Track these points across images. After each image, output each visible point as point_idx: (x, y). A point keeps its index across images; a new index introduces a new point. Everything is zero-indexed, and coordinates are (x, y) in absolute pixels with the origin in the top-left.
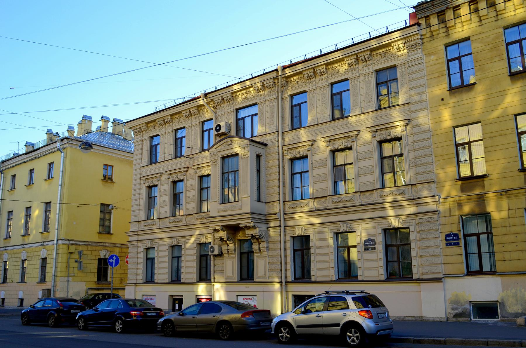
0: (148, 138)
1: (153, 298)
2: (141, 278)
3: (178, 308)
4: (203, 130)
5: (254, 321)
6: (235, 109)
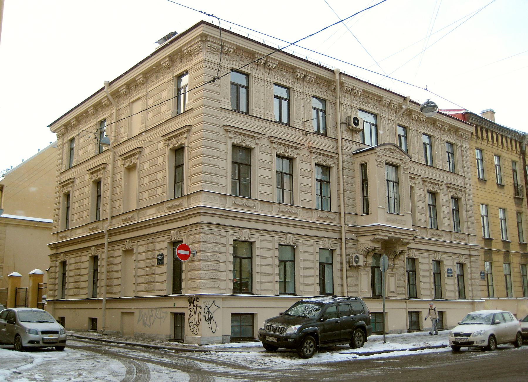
6: (175, 76)
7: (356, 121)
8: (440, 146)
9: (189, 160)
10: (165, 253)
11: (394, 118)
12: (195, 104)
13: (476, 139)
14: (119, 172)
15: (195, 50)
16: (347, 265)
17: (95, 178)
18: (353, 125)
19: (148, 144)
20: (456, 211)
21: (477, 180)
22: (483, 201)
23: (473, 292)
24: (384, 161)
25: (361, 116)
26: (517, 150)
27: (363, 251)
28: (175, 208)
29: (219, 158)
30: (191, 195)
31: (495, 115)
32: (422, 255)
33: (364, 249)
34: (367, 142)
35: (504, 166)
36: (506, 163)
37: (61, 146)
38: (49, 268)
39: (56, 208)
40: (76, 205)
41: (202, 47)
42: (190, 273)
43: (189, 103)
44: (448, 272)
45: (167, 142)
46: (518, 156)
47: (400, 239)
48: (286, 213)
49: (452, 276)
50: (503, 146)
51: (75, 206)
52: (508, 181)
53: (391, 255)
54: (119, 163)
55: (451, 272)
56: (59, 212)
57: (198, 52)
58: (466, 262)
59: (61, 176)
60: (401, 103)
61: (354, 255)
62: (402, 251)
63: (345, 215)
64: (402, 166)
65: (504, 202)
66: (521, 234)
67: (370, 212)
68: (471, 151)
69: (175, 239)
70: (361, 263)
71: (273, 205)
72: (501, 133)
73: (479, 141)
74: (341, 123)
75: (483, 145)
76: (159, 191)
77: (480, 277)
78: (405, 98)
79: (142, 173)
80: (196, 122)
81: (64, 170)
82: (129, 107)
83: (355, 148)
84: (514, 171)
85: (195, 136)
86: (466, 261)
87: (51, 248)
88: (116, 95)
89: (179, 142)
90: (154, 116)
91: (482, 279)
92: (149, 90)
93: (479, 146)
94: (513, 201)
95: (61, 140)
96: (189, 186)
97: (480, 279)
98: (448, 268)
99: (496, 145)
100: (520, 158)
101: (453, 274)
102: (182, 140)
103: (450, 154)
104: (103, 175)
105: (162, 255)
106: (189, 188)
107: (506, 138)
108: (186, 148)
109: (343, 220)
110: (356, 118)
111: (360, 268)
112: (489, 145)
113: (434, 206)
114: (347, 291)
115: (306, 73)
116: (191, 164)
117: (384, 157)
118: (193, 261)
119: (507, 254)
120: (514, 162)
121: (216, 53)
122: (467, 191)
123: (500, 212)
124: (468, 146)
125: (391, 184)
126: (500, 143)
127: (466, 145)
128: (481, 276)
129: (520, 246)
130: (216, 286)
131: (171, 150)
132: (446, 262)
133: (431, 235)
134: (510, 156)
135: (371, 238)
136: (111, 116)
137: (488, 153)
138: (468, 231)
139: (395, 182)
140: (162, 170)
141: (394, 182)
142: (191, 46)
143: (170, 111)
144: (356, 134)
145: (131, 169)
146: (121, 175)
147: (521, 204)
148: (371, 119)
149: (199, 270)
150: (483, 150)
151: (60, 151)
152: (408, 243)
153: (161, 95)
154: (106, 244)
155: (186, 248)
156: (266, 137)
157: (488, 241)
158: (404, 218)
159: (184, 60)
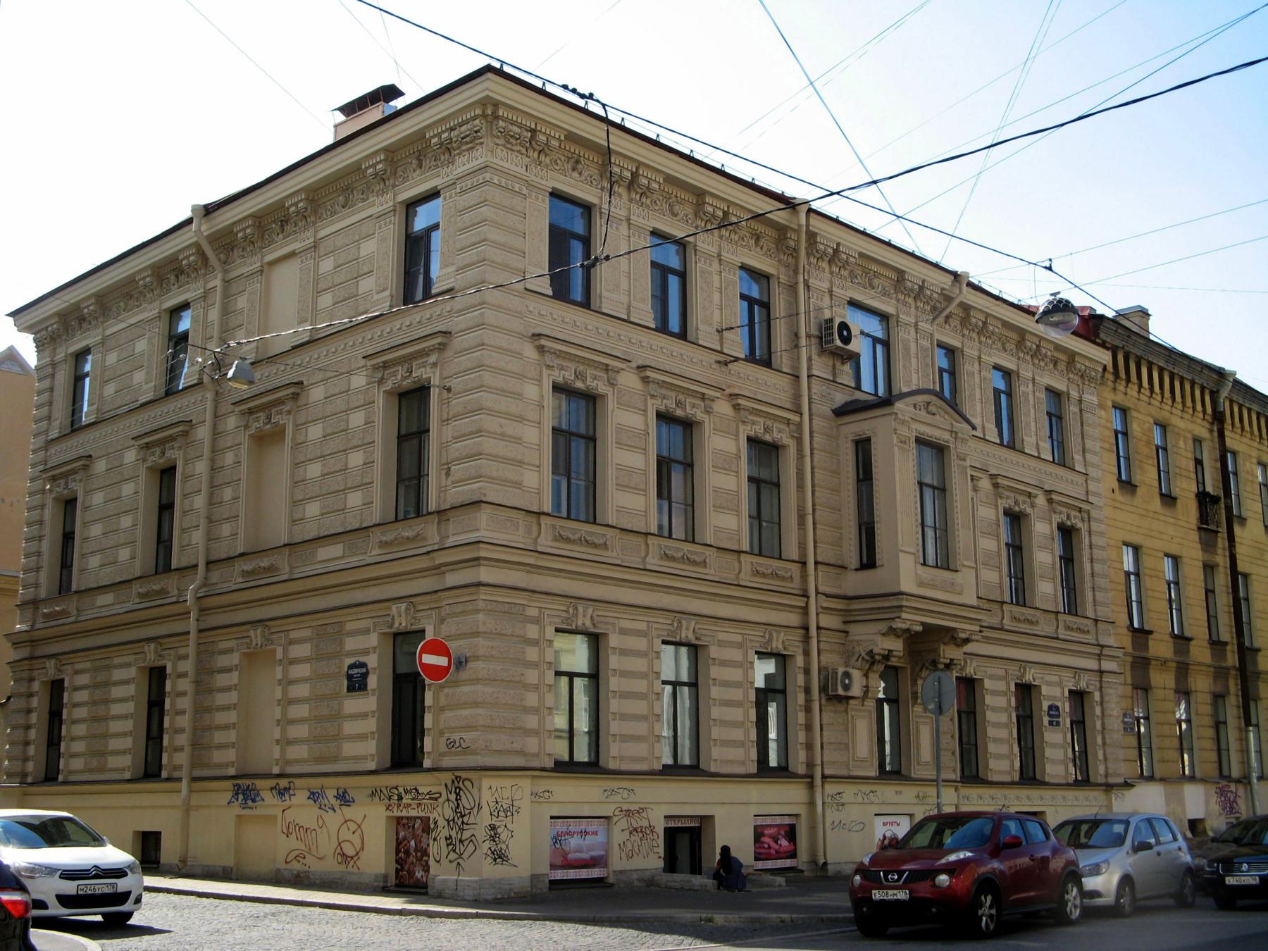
0: (394, 206)
1: (590, 829)
2: (124, 761)
3: (1227, 882)
4: (409, 232)
5: (1064, 853)
6: (401, 203)
7: (845, 333)
8: (1031, 397)
9: (445, 421)
10: (372, 661)
11: (929, 327)
12: (463, 277)
13: (1114, 382)
14: (229, 445)
15: (463, 138)
16: (822, 695)
17: (156, 459)
18: (838, 343)
19: (320, 375)
20: (1068, 559)
21: (1115, 485)
22: (1130, 538)
23: (1106, 765)
24: (914, 434)
25: (858, 322)
26: (1204, 412)
27: (860, 658)
28: (400, 544)
29: (520, 419)
30: (450, 514)
31: (1150, 322)
32: (1048, 678)
33: (863, 654)
34: (867, 385)
35: (1175, 450)
36: (1181, 444)
37: (50, 370)
38: (9, 699)
39: (30, 536)
40: (96, 530)
41: (483, 132)
42: (448, 714)
43: (442, 274)
44: (1051, 712)
45: (380, 375)
46: (1207, 425)
47: (954, 629)
48: (679, 563)
49: (1058, 724)
50: (1163, 397)
51: (90, 532)
52: (1185, 489)
53: (924, 671)
54: (231, 422)
55: (1057, 713)
56: (40, 547)
57: (470, 145)
58: (1091, 689)
59: (47, 450)
60: (947, 288)
61: (841, 670)
62: (952, 660)
63: (816, 569)
64: (955, 449)
65: (1176, 540)
66: (1213, 620)
67: (878, 563)
68: (1103, 413)
69: (402, 623)
70: (856, 690)
71: (650, 542)
72: (1170, 368)
73: (1121, 386)
74: (808, 336)
75: (1130, 395)
76: (355, 499)
77: (1121, 726)
78: (955, 275)
79: (300, 452)
80: (463, 326)
81: (57, 435)
82: (261, 275)
83: (840, 398)
84: (1199, 462)
85: (464, 361)
86: (1090, 687)
87: (14, 644)
88: (226, 243)
89: (414, 375)
90: (336, 304)
91: (1052, 725)
92: (322, 234)
93: (1120, 398)
94: (1195, 536)
95: (47, 353)
96: (443, 489)
97: (1122, 732)
98: (1050, 703)
99: (1159, 398)
100: (1211, 431)
101: (1061, 720)
102: (423, 369)
103: (1054, 419)
104: (181, 453)
105: (363, 665)
106: (443, 494)
107: (1182, 380)
108: (434, 393)
109: (811, 580)
110: (844, 326)
111: (851, 702)
112: (1142, 397)
113: (1017, 549)
114: (822, 762)
115: (728, 207)
116: (449, 432)
117: (915, 426)
118: (455, 684)
119: (1183, 670)
120: (1197, 441)
121: (518, 148)
122: (1094, 513)
123: (1167, 564)
124: (1094, 399)
125: (928, 493)
126: (1167, 394)
127: (1091, 398)
128: (1125, 723)
129: (1211, 648)
130: (517, 746)
131: (388, 393)
132: (1045, 690)
133: (1012, 621)
134: (1191, 426)
135: (883, 626)
136: (205, 297)
137: (1140, 416)
138: (1095, 610)
139: (938, 489)
140: (362, 446)
141: (934, 488)
142: (452, 129)
143: (387, 293)
144: (843, 363)
145: (266, 440)
146: (237, 456)
147: (1215, 545)
148: (874, 327)
149: (476, 704)
150: (1129, 408)
151: (47, 383)
152: (967, 641)
153: (359, 248)
154: (193, 636)
155: (438, 648)
156: (631, 368)
157: (1141, 634)
158: (958, 578)
159: (426, 163)
